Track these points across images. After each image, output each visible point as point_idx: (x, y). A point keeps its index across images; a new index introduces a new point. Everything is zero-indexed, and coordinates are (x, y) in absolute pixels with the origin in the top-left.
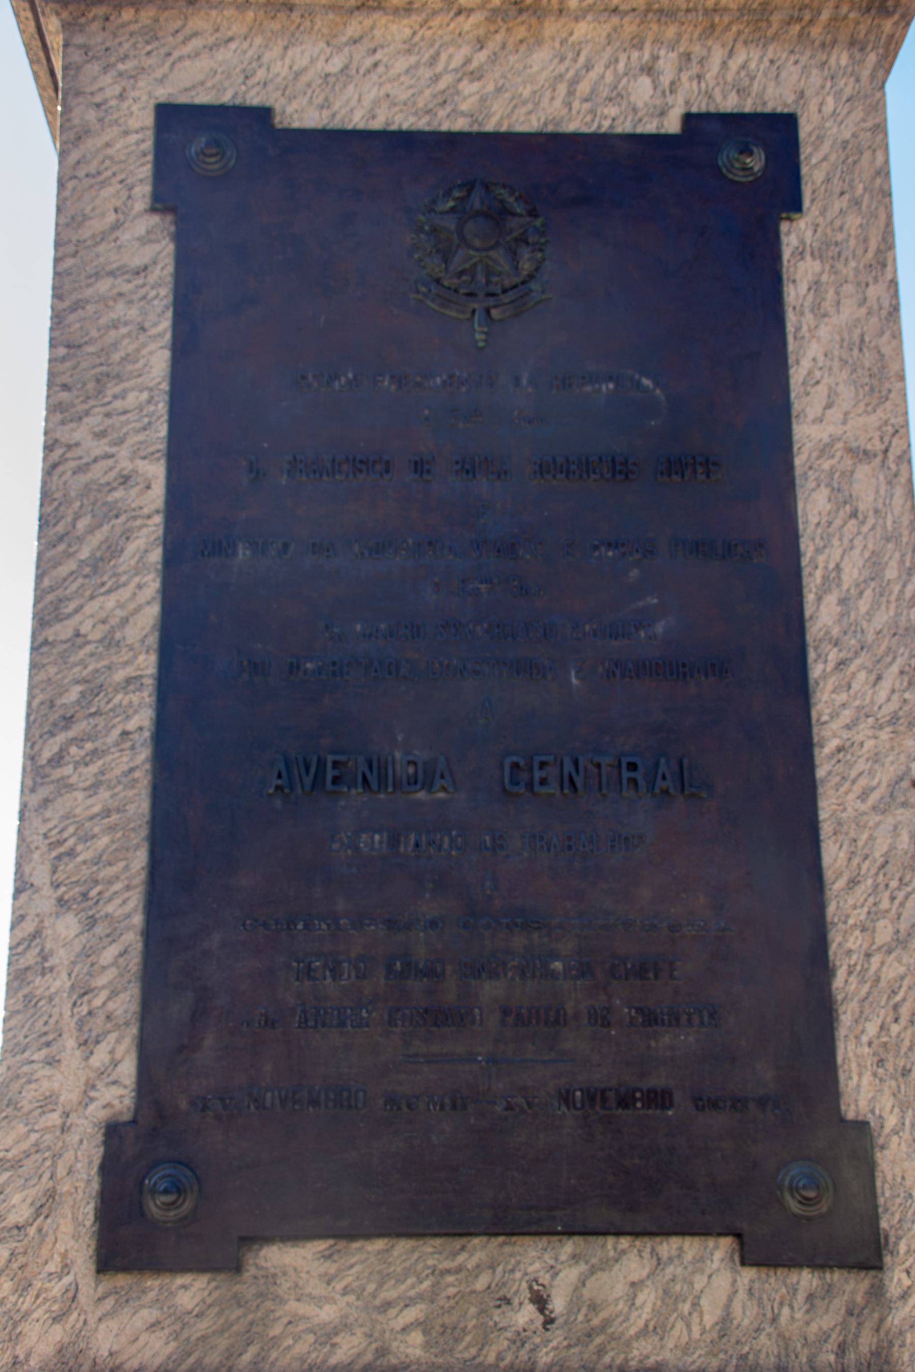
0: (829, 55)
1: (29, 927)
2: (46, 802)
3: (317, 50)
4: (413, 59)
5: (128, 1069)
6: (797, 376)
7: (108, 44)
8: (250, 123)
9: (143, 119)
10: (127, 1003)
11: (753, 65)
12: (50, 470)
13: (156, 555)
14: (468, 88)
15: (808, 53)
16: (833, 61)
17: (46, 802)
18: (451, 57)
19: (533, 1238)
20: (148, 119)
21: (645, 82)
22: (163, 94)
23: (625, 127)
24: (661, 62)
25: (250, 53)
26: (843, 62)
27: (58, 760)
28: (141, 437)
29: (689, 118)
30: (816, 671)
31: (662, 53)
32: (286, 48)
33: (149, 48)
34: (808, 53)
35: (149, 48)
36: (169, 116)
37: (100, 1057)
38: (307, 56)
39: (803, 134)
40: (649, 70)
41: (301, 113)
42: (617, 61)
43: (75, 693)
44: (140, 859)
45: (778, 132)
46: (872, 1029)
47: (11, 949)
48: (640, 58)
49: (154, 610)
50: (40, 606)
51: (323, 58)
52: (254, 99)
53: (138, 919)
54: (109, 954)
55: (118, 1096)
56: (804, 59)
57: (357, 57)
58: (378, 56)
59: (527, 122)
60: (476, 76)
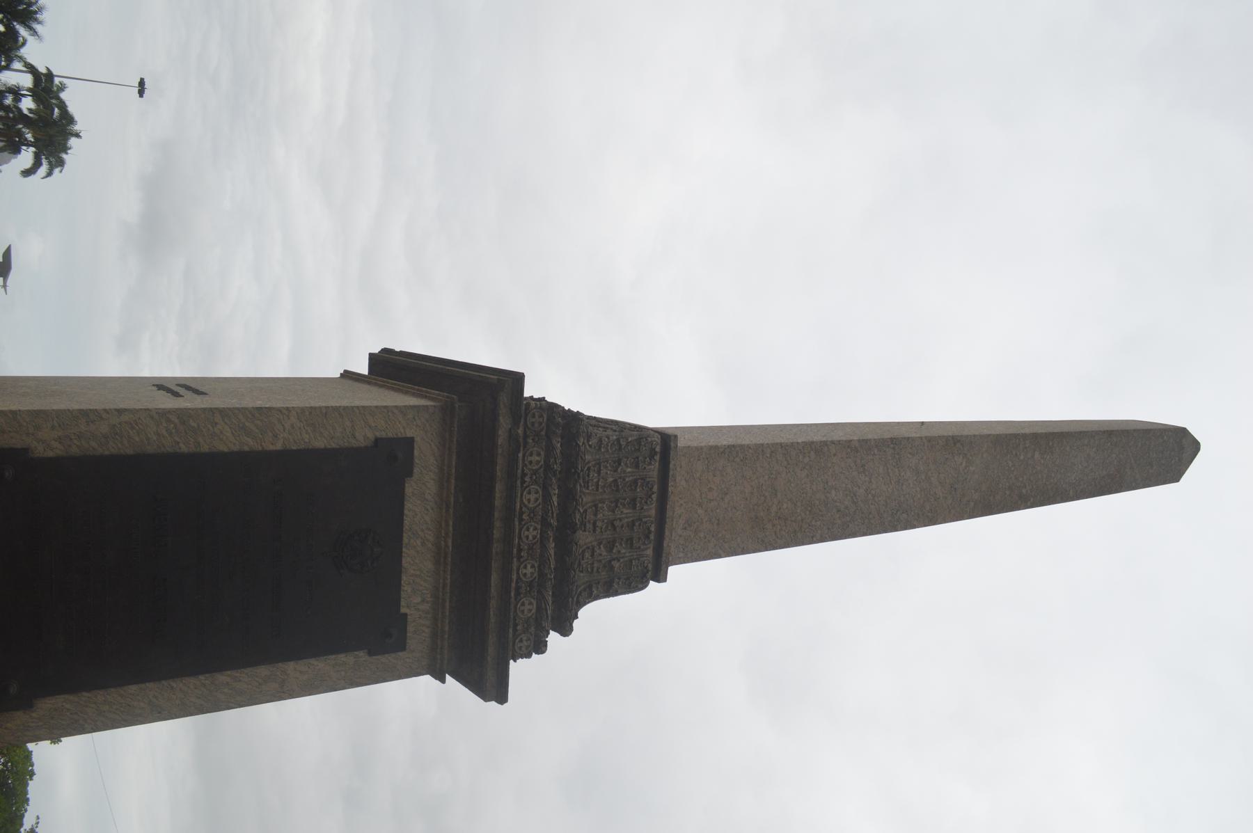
1: (104, 415)
2: (152, 417)
5: (51, 454)
6: (313, 661)
8: (408, 470)
9: (409, 433)
10: (75, 451)
12: (279, 410)
13: (246, 448)
14: (419, 542)
17: (152, 417)
19: (350, 382)
20: (409, 434)
21: (419, 599)
22: (418, 439)
23: (403, 595)
27: (169, 421)
29: (406, 615)
30: (202, 677)
36: (410, 442)
37: (55, 444)
39: (400, 654)
40: (423, 601)
41: (410, 488)
43: (194, 424)
44: (130, 451)
45: (401, 646)
46: (68, 706)
49: (226, 450)
52: (416, 470)
53: (107, 453)
54: (93, 444)
55: (40, 451)
59: (406, 561)
60: (423, 544)
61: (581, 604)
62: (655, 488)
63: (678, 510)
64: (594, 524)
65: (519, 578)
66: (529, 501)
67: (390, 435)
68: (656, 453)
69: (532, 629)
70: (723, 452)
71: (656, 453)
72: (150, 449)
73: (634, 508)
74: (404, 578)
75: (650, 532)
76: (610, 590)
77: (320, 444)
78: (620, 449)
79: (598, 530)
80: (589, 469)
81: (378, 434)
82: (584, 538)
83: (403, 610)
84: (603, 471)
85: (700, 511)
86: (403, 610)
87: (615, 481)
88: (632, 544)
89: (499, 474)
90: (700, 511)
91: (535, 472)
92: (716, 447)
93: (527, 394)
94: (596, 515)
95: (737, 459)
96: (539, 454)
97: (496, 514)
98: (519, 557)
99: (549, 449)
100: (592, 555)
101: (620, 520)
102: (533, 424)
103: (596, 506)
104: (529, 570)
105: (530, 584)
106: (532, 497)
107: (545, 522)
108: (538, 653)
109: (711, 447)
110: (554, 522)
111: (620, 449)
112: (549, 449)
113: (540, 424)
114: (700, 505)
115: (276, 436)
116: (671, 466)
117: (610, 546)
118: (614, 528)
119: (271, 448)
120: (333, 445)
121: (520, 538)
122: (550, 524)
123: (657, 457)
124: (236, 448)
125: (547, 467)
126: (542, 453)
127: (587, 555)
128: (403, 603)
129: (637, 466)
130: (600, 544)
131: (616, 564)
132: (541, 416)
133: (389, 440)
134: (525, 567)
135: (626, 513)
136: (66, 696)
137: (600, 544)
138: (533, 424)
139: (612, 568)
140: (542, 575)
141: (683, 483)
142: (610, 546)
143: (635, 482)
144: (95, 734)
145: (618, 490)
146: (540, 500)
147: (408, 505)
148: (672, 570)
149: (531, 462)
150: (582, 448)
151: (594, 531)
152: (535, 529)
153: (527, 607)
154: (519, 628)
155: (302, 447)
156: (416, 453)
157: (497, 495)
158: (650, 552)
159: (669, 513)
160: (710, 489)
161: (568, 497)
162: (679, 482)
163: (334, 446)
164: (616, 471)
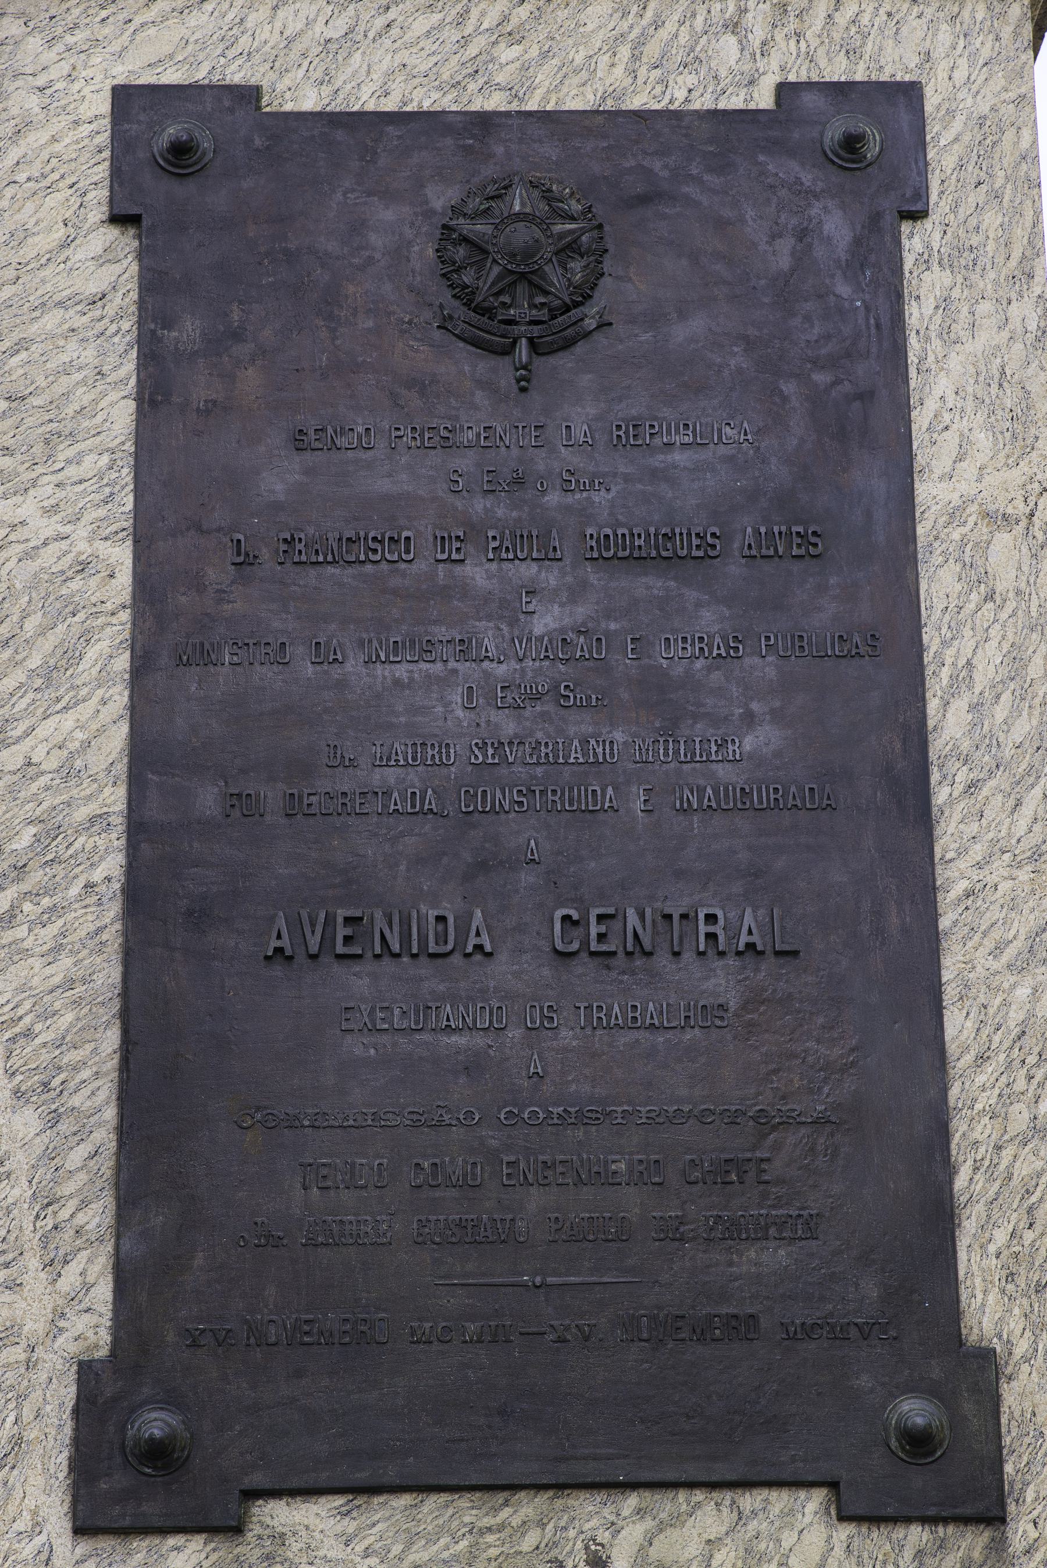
5: (104, 1292)
6: (921, 419)
11: (865, 19)
13: (123, 662)
14: (507, 53)
16: (966, 14)
18: (483, 14)
21: (730, 43)
22: (122, 73)
23: (702, 102)
24: (750, 15)
25: (230, 16)
26: (979, 16)
29: (783, 89)
33: (104, 14)
35: (104, 14)
36: (126, 99)
37: (70, 1278)
42: (694, 15)
44: (111, 1039)
46: (1001, 1236)
51: (322, 20)
52: (236, 76)
53: (110, 1114)
54: (77, 1156)
58: (392, 14)
60: (515, 37)
67: (102, 171)
72: (108, 974)
74: (636, 103)
77: (120, 415)
81: (97, 213)
83: (764, 99)
86: (764, 99)
115: (83, 567)
119: (125, 578)
120: (127, 369)
124: (120, 697)
128: (735, 102)
133: (116, 173)
136: (963, 1243)
144: (622, 1525)
147: (366, 100)
155: (126, 475)
156: (171, 77)
163: (130, 366)
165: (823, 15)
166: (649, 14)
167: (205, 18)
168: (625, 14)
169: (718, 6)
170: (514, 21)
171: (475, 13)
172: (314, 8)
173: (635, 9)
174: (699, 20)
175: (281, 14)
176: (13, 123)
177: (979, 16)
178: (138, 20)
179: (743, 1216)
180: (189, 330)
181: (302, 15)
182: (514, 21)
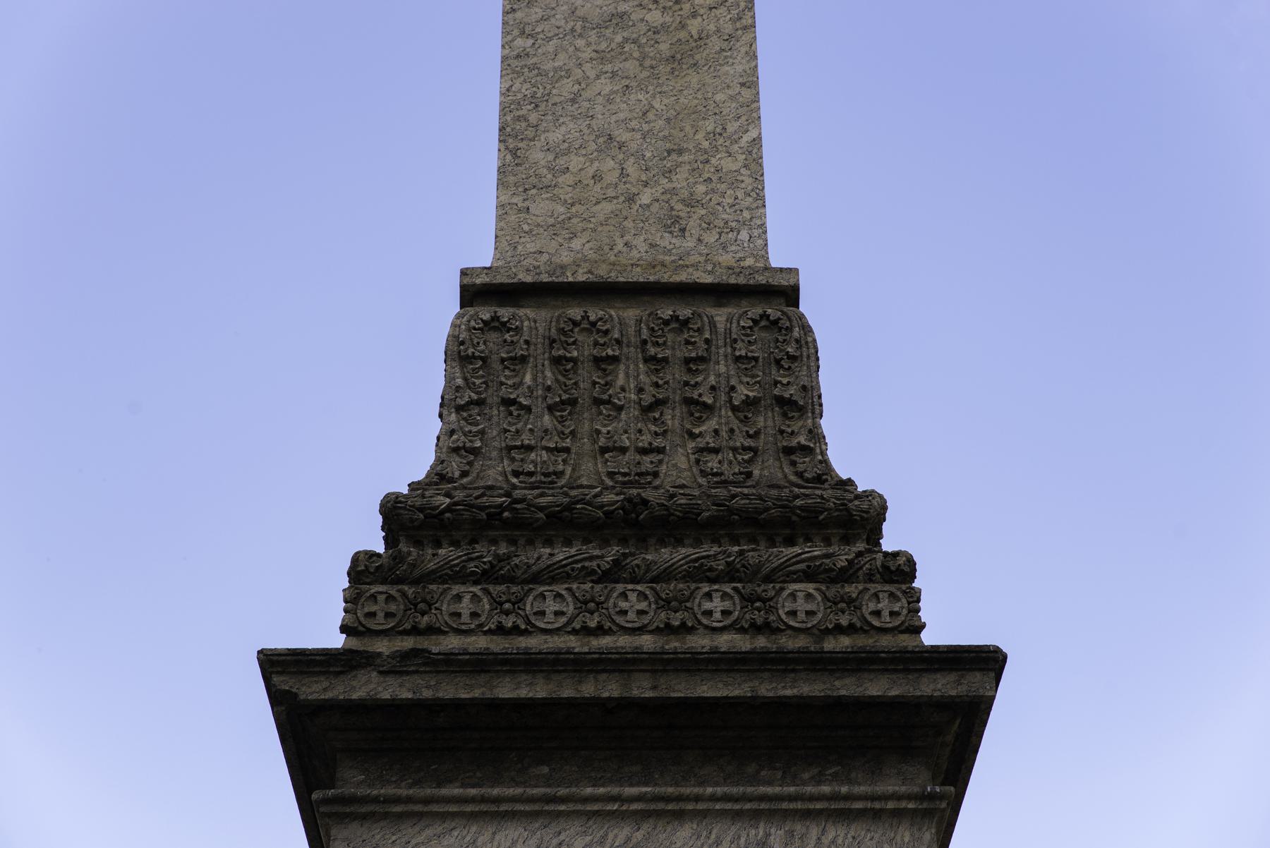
0: (896, 833)
3: (517, 833)
4: (588, 838)
7: (364, 837)
11: (840, 841)
15: (880, 832)
16: (898, 838)
18: (616, 836)
24: (772, 838)
25: (468, 838)
26: (906, 840)
28: (543, 478)
31: (773, 831)
32: (494, 834)
33: (394, 838)
34: (880, 832)
35: (394, 838)
38: (510, 838)
42: (739, 838)
47: (502, 94)
48: (756, 835)
50: (753, 134)
51: (521, 840)
56: (877, 836)
57: (547, 838)
58: (562, 837)
61: (824, 474)
62: (575, 312)
63: (637, 251)
64: (644, 451)
65: (735, 627)
66: (558, 614)
68: (495, 318)
69: (852, 590)
70: (514, 153)
71: (495, 318)
73: (615, 360)
75: (675, 318)
76: (802, 405)
78: (480, 403)
79: (658, 442)
80: (516, 474)
82: (678, 470)
84: (527, 439)
85: (645, 199)
87: (551, 409)
88: (701, 359)
89: (477, 693)
90: (645, 199)
91: (497, 603)
92: (502, 171)
93: (337, 641)
94: (623, 450)
95: (533, 118)
96: (458, 598)
97: (567, 693)
98: (685, 629)
99: (699, 573)
100: (716, 451)
101: (640, 390)
102: (389, 615)
103: (604, 450)
104: (717, 605)
105: (748, 600)
106: (551, 606)
107: (609, 576)
108: (912, 575)
109: (502, 184)
110: (614, 551)
111: (480, 403)
112: (699, 573)
113: (390, 598)
114: (631, 199)
116: (529, 279)
117: (698, 408)
118: (658, 403)
121: (640, 630)
122: (616, 562)
123: (505, 313)
125: (488, 576)
126: (457, 589)
127: (712, 463)
129: (523, 359)
130: (693, 436)
131: (743, 392)
132: (374, 597)
134: (709, 613)
135: (629, 379)
137: (693, 436)
138: (389, 615)
139: (750, 403)
140: (731, 574)
141: (576, 244)
142: (698, 408)
143: (557, 361)
145: (573, 402)
146: (561, 588)
148: (777, 259)
149: (474, 615)
150: (459, 495)
151: (660, 450)
152: (624, 595)
153: (801, 605)
154: (844, 621)
157: (524, 693)
158: (720, 315)
159: (637, 276)
160: (597, 177)
161: (565, 522)
162: (572, 257)
164: (528, 409)
165: (815, 838)
166: (713, 836)
167: (453, 840)
168: (699, 837)
169: (753, 832)
170: (634, 840)
171: (611, 836)
172: (517, 833)
173: (705, 833)
174: (743, 840)
175: (497, 837)
176: (785, 309)
177: (906, 840)
178: (414, 842)
179: (626, 40)
180: (760, 242)
181: (510, 838)
182: (634, 840)
